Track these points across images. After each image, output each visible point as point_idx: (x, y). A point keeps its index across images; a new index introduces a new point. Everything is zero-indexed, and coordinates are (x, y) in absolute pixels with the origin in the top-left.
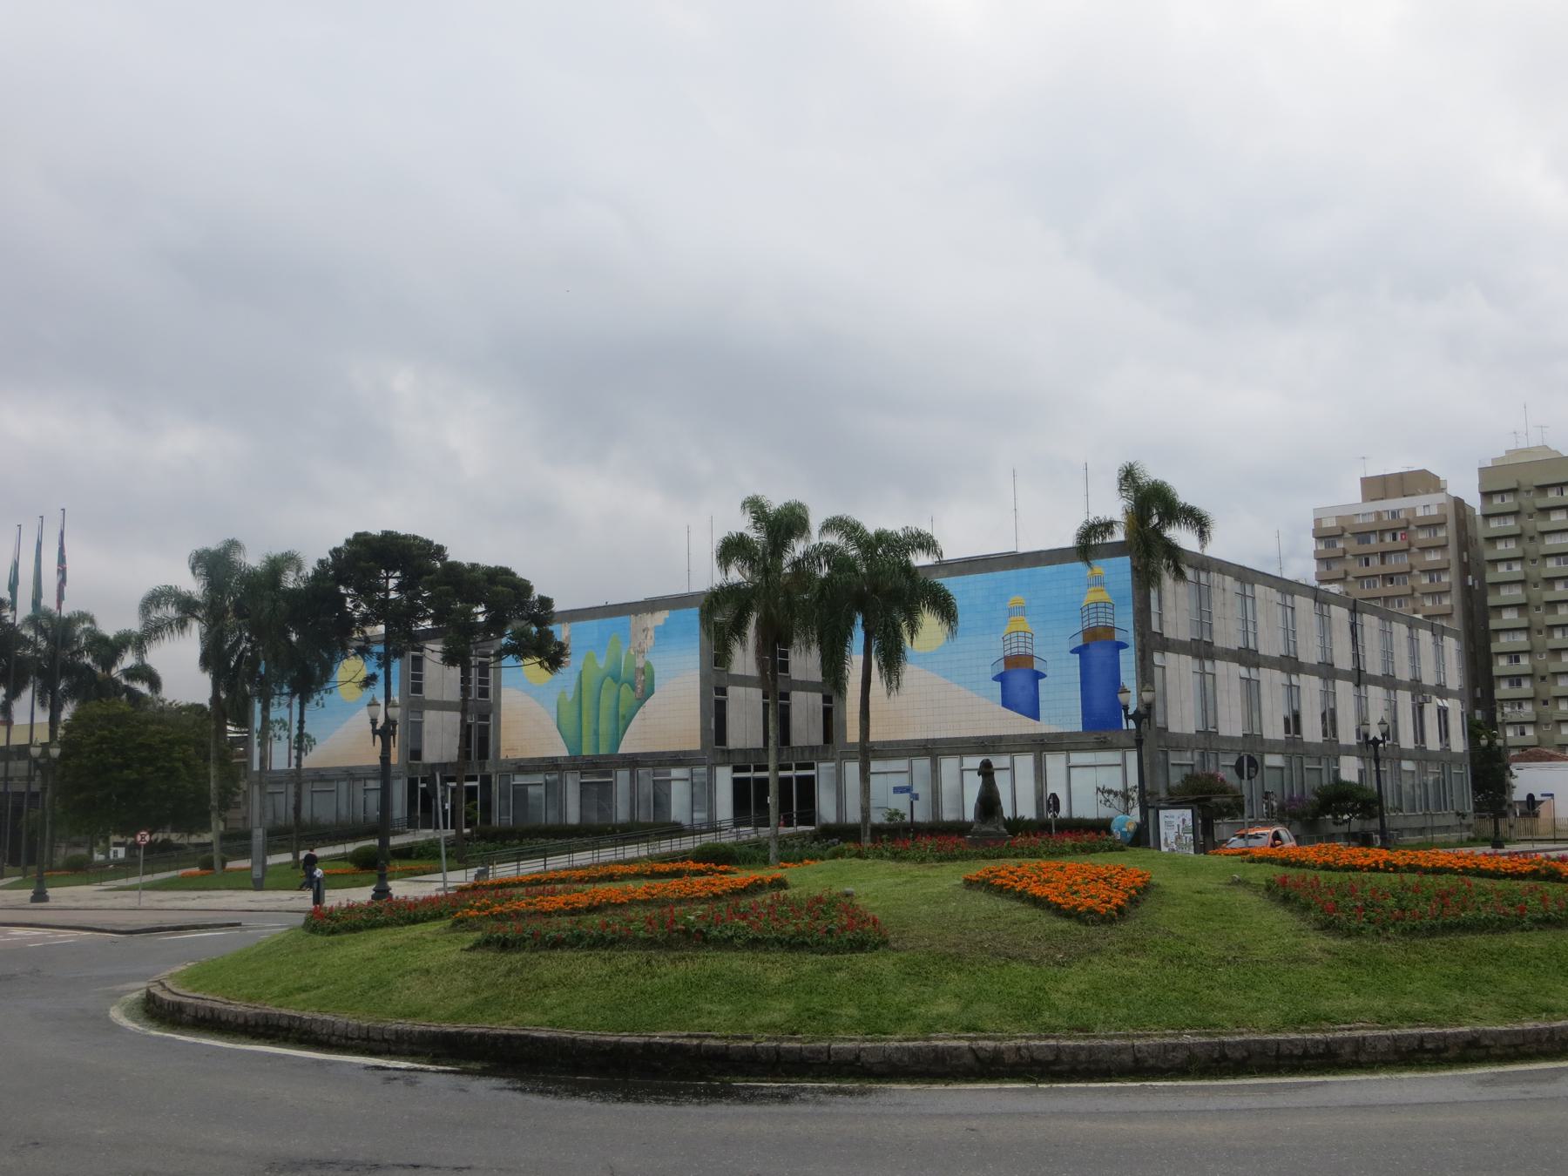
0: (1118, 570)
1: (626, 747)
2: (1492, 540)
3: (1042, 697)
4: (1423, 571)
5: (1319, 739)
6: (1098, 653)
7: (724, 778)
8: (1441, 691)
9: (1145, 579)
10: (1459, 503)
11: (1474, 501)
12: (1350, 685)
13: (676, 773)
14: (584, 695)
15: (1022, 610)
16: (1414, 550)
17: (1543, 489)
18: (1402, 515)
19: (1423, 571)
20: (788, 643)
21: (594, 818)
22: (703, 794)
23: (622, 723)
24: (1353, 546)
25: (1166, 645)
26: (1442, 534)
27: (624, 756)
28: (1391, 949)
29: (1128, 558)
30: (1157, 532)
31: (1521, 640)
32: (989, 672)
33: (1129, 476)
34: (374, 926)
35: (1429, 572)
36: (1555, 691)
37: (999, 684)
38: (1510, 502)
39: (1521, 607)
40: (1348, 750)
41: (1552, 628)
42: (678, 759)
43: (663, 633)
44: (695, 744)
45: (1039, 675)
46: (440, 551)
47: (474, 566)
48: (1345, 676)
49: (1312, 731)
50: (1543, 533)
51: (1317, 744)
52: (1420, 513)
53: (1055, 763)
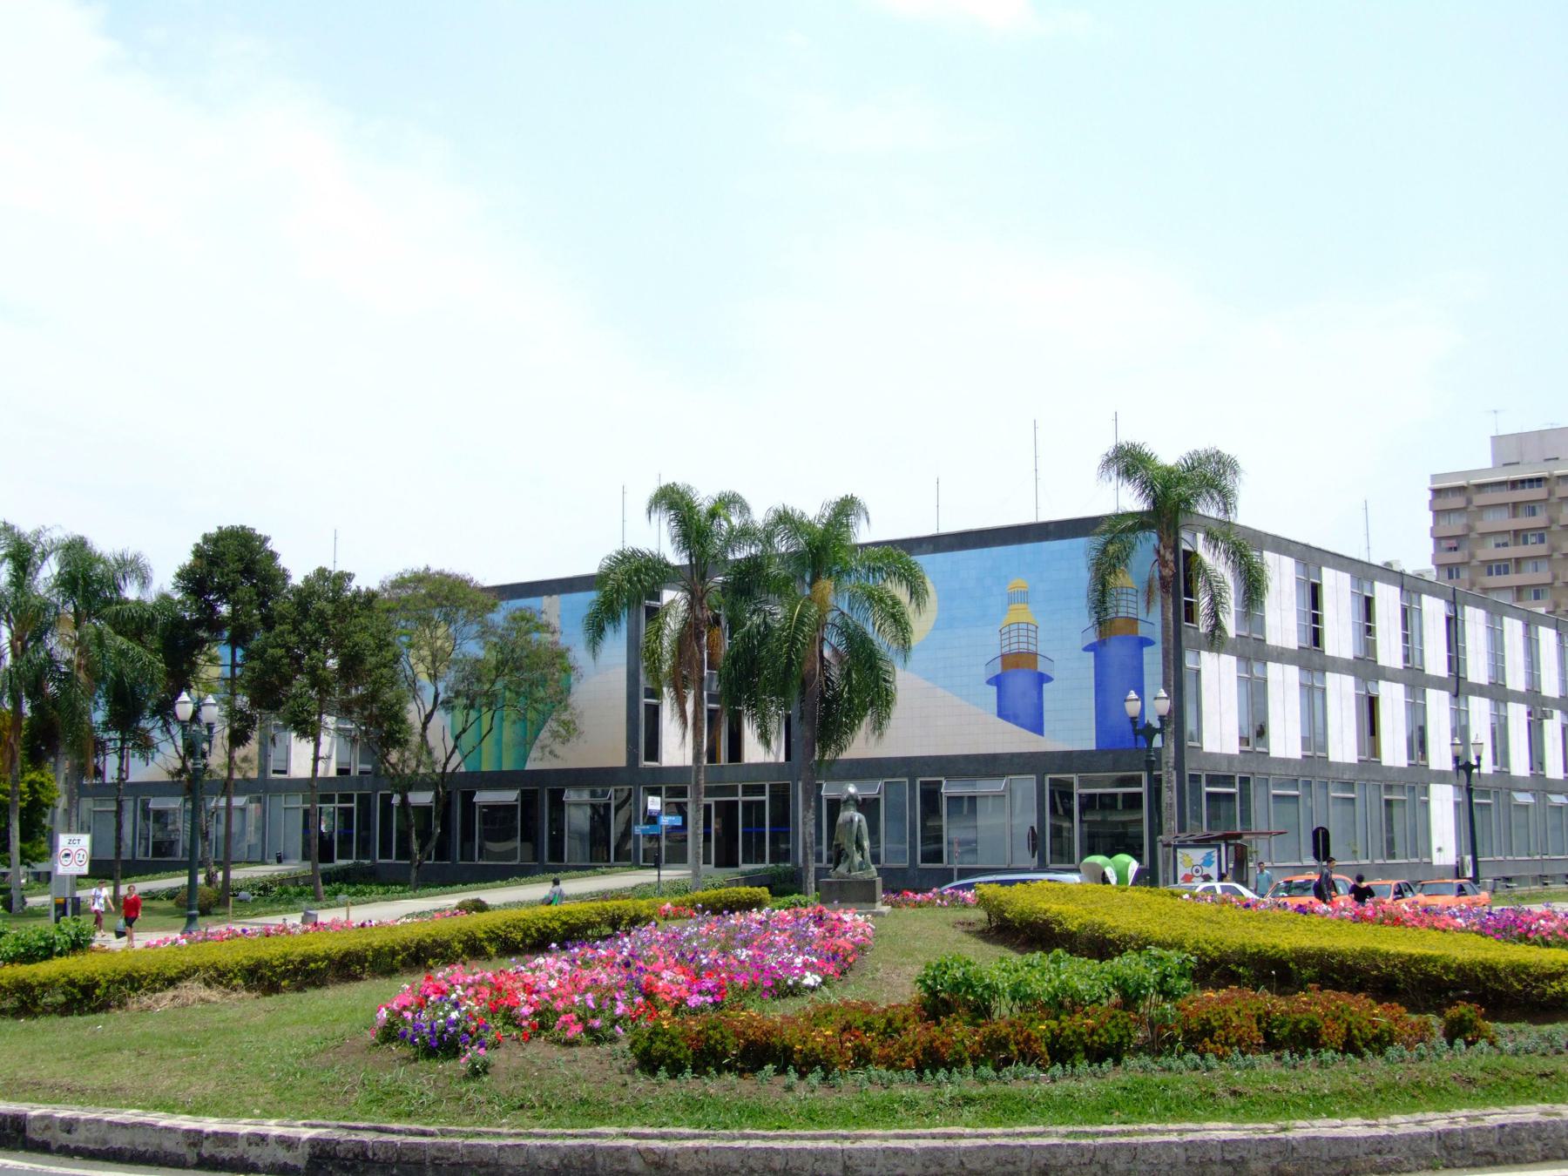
3: (1047, 706)
5: (1402, 761)
12: (1445, 696)
15: (1023, 597)
16: (1471, 508)
32: (982, 673)
37: (994, 689)
40: (1441, 777)
45: (1043, 679)
48: (1438, 683)
49: (1394, 752)
51: (1400, 769)
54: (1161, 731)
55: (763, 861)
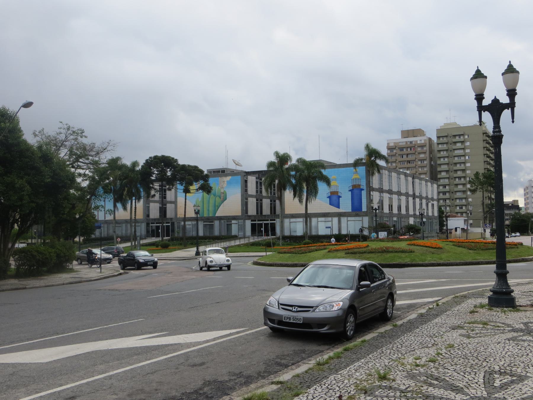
0: (362, 170)
1: (218, 214)
2: (439, 151)
4: (419, 160)
6: (356, 192)
7: (248, 223)
8: (432, 199)
9: (369, 174)
10: (430, 139)
11: (435, 139)
13: (233, 222)
14: (205, 200)
16: (417, 153)
17: (455, 136)
18: (413, 143)
19: (419, 160)
20: (285, 189)
21: (208, 234)
22: (242, 228)
23: (216, 208)
24: (399, 152)
25: (373, 190)
26: (425, 149)
27: (217, 217)
28: (481, 252)
29: (364, 167)
30: (374, 161)
31: (446, 181)
32: (326, 196)
33: (367, 147)
34: (288, 253)
35: (422, 160)
36: (456, 197)
38: (445, 140)
39: (447, 171)
41: (455, 178)
42: (235, 218)
43: (229, 183)
44: (240, 214)
45: (340, 197)
46: (176, 161)
47: (189, 165)
48: (411, 196)
49: (403, 211)
50: (454, 150)
52: (419, 142)
53: (344, 220)
54: (378, 209)
55: (268, 236)
